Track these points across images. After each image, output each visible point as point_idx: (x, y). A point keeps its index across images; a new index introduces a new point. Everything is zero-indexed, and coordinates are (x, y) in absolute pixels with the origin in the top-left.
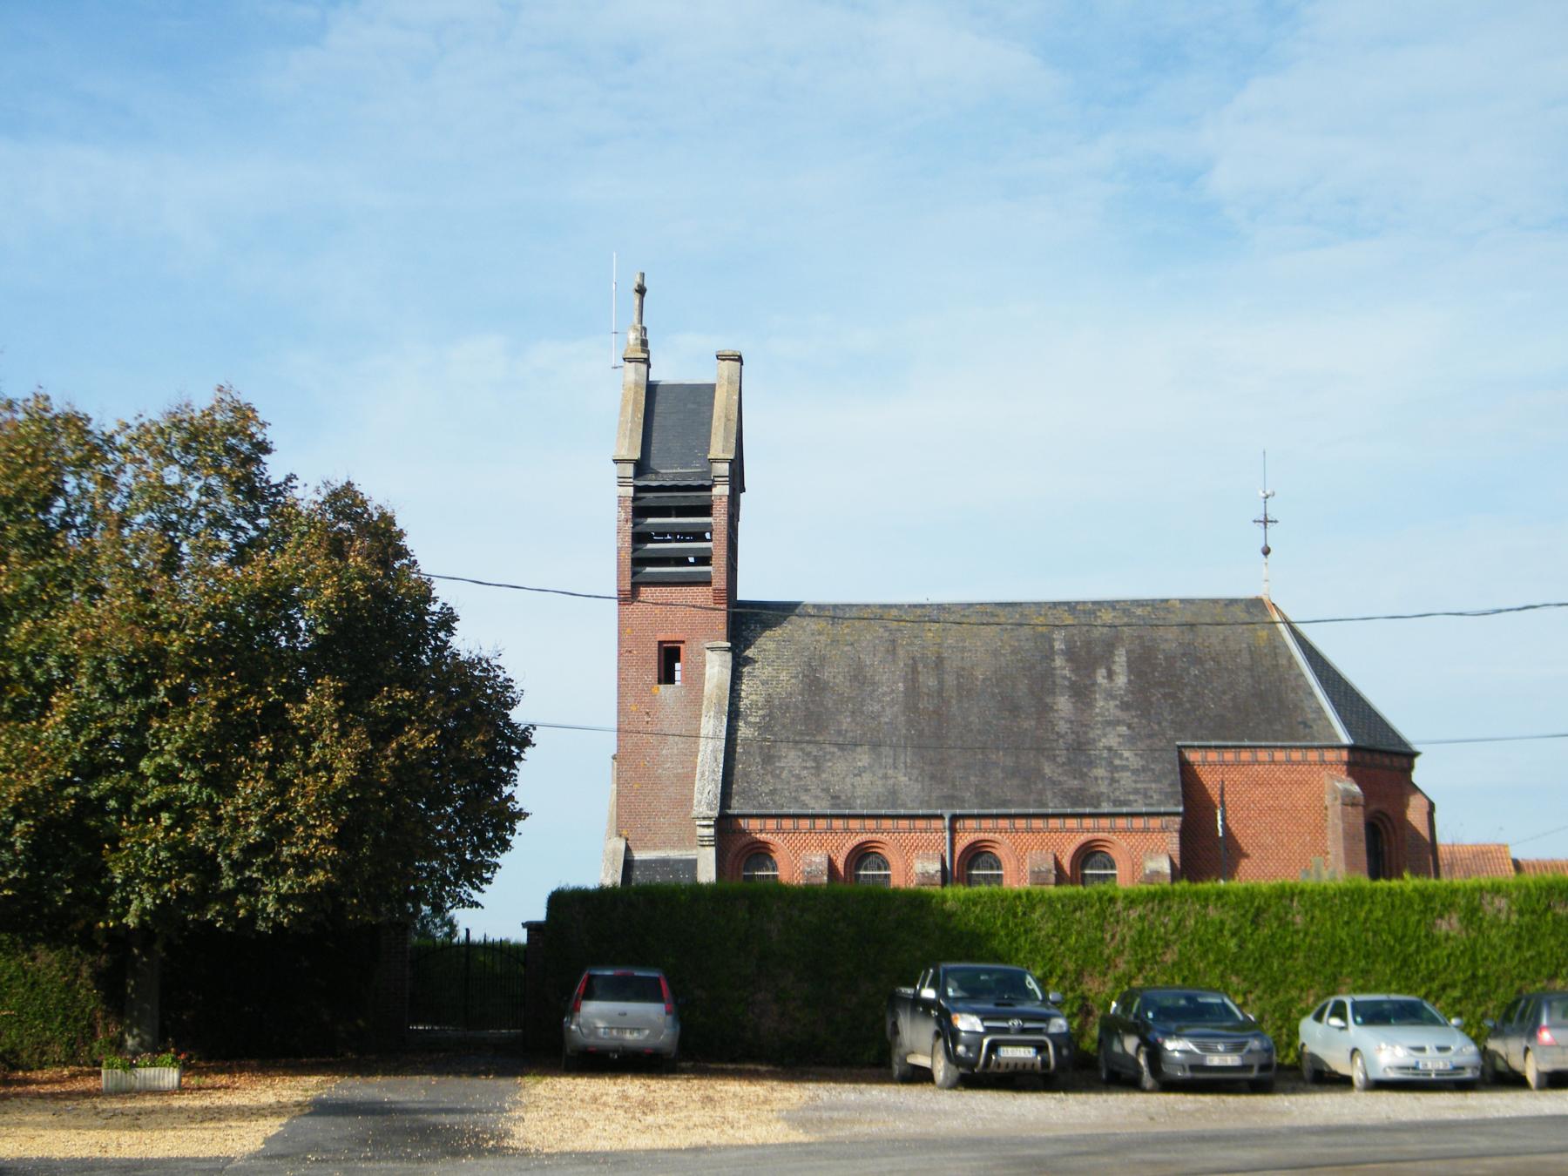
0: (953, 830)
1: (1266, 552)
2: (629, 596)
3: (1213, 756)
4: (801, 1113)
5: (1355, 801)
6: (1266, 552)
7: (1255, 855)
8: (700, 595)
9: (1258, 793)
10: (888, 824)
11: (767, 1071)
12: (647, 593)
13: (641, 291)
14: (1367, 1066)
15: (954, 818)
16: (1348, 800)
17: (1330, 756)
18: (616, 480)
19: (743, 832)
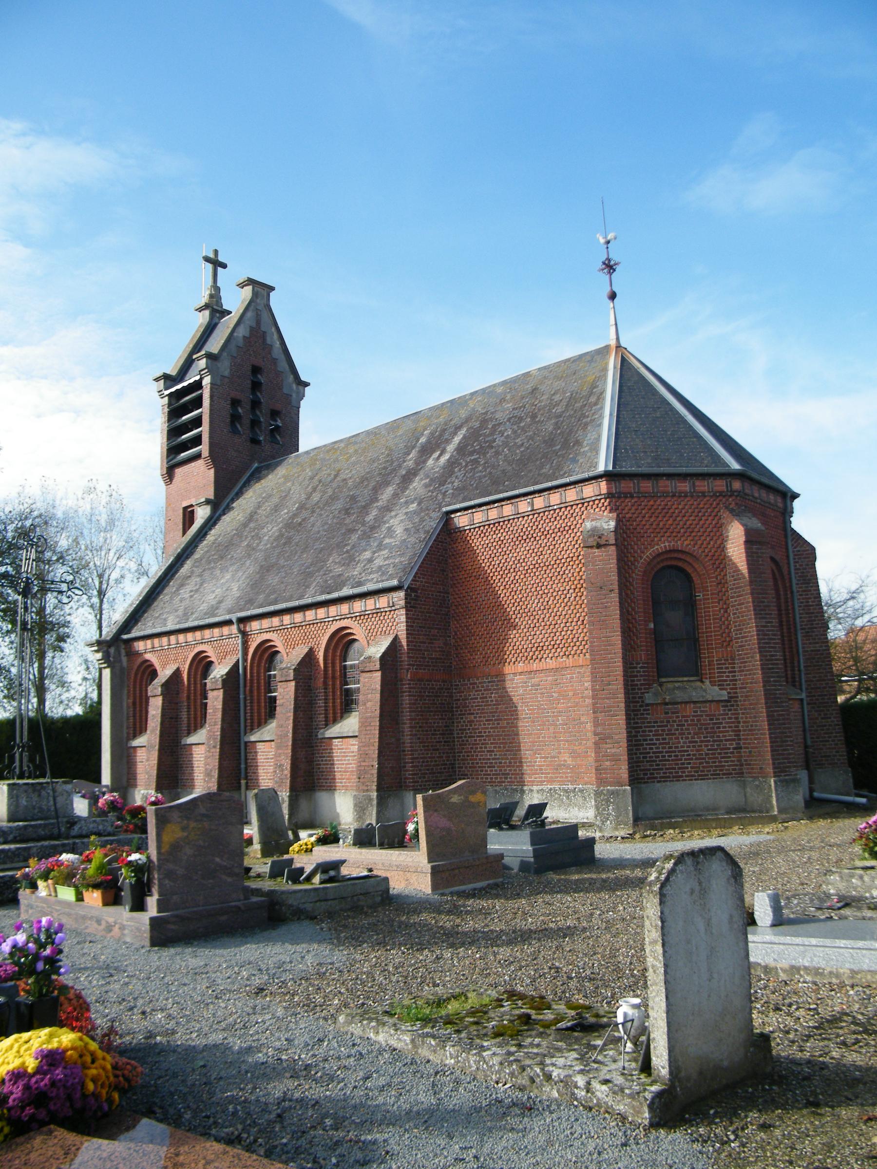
0: (244, 634)
1: (613, 296)
2: (169, 474)
3: (479, 517)
4: (869, 977)
5: (603, 542)
6: (613, 296)
7: (522, 622)
8: (200, 463)
9: (522, 550)
10: (207, 633)
11: (417, 912)
12: (179, 472)
13: (609, 267)
14: (742, 944)
15: (242, 620)
16: (592, 541)
17: (589, 491)
18: (158, 394)
19: (138, 654)
